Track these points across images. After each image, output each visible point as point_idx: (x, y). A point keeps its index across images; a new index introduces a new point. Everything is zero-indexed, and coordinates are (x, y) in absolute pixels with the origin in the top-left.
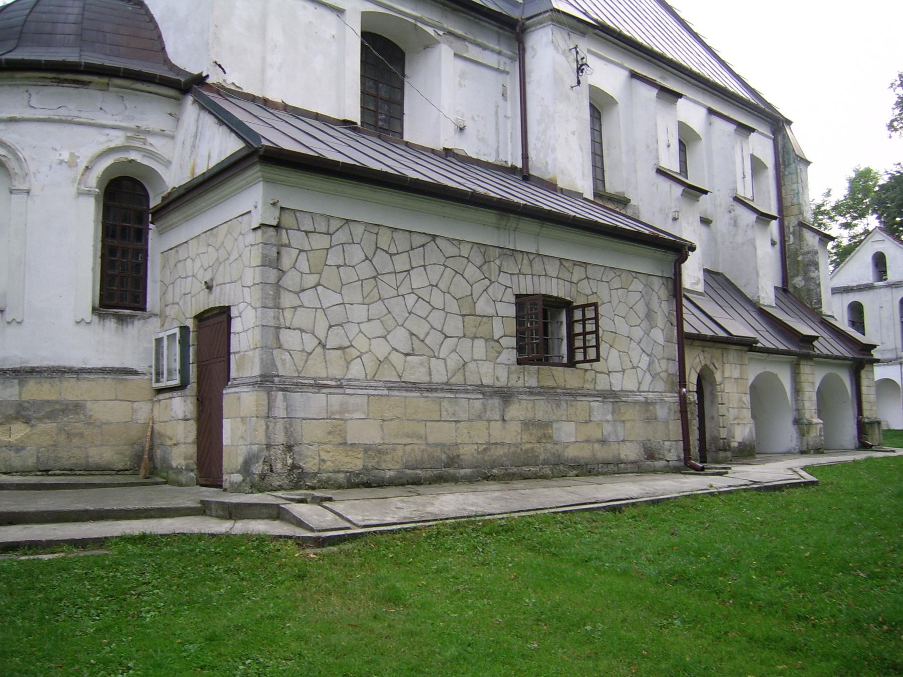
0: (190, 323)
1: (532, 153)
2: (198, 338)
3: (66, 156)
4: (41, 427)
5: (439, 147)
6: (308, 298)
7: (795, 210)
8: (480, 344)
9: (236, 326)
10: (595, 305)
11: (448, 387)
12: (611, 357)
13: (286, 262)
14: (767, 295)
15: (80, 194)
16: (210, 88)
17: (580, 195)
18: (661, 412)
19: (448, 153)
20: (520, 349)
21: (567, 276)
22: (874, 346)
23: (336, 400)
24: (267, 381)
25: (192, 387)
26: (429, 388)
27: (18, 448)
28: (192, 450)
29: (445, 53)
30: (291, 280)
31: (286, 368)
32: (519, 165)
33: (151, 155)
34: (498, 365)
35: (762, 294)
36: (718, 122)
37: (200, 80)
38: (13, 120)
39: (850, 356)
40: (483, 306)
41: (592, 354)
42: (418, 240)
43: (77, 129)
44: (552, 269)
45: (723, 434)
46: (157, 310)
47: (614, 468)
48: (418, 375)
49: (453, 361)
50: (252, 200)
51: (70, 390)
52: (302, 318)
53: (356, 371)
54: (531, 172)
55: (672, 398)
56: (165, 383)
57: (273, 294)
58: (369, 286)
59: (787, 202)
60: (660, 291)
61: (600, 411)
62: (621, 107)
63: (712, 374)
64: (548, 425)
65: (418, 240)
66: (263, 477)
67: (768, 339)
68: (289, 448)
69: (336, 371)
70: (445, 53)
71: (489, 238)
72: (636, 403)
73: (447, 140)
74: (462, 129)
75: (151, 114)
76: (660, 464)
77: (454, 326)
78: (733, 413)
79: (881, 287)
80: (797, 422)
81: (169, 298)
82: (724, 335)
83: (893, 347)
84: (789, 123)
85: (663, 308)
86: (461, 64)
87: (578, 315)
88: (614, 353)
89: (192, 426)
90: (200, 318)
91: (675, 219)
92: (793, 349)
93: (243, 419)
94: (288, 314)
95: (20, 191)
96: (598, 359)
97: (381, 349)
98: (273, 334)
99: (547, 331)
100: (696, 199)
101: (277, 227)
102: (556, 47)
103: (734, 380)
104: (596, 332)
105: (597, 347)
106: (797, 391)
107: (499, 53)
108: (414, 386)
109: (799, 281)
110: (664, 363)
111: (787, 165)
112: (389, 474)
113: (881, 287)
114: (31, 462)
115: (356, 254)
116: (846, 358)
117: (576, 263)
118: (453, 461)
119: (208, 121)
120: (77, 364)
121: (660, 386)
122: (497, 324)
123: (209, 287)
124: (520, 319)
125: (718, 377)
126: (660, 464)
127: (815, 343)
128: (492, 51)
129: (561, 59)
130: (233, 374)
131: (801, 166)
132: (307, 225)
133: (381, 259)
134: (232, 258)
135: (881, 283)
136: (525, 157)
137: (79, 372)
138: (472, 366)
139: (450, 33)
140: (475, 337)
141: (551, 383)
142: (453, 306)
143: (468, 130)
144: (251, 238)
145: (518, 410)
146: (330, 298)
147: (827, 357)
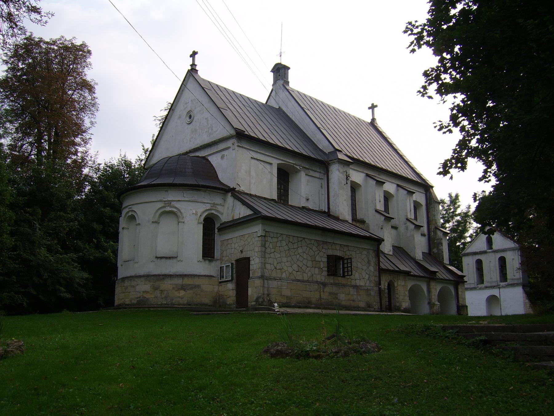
0: (234, 262)
1: (331, 207)
2: (236, 268)
3: (194, 212)
4: (188, 292)
5: (301, 206)
6: (272, 255)
7: (434, 223)
8: (317, 269)
9: (252, 262)
10: (351, 258)
11: (308, 281)
12: (356, 275)
13: (267, 246)
14: (419, 256)
15: (199, 223)
16: (236, 192)
17: (347, 221)
18: (372, 293)
19: (304, 208)
20: (328, 271)
21: (342, 249)
22: (465, 276)
23: (279, 283)
24: (262, 277)
25: (235, 280)
26: (302, 281)
27: (182, 298)
28: (234, 298)
29: (303, 174)
30: (268, 250)
31: (267, 274)
32: (327, 211)
33: (217, 211)
34: (322, 276)
35: (417, 256)
36: (401, 190)
37: (234, 189)
38: (179, 201)
39: (452, 279)
40: (318, 258)
41: (350, 273)
42: (300, 239)
43: (196, 203)
44: (338, 247)
45: (398, 304)
46: (219, 258)
47: (358, 308)
48: (300, 278)
49: (309, 274)
50: (258, 229)
51: (197, 281)
52: (270, 261)
53: (284, 275)
54: (331, 214)
55: (376, 289)
56: (224, 279)
57: (264, 254)
58: (287, 252)
59: (431, 219)
60: (372, 255)
61: (352, 291)
62: (363, 189)
63: (393, 283)
64: (336, 294)
65: (300, 239)
66: (262, 302)
67: (416, 271)
68: (268, 295)
69: (279, 275)
70: (303, 174)
71: (319, 238)
72: (364, 289)
73: (303, 203)
74: (308, 200)
75: (218, 199)
76: (372, 309)
77: (310, 264)
78: (401, 298)
79: (490, 252)
80: (429, 303)
81: (225, 254)
82: (398, 270)
83: (496, 280)
84: (432, 187)
85: (373, 260)
86: (308, 177)
87: (346, 261)
88: (357, 274)
89: (235, 291)
90: (237, 261)
91: (382, 228)
92: (426, 275)
93: (256, 287)
94: (267, 260)
95: (181, 222)
96: (352, 275)
97: (290, 270)
98: (263, 267)
99: (337, 266)
100: (390, 221)
101: (265, 236)
102: (339, 171)
103: (402, 288)
104: (351, 267)
105: (351, 271)
106: (429, 291)
107: (320, 173)
108: (299, 281)
109: (435, 250)
110: (373, 278)
111: (431, 204)
112: (293, 304)
113: (490, 252)
114: (186, 302)
115: (284, 243)
116: (451, 280)
117: (345, 246)
118: (310, 302)
119: (238, 204)
120: (198, 274)
121: (372, 285)
122: (321, 263)
123: (242, 252)
124: (328, 262)
125: (396, 284)
126: (372, 309)
127: (437, 274)
128: (318, 172)
129: (341, 175)
130: (251, 276)
131: (437, 205)
132: (272, 235)
133: (290, 244)
134: (250, 244)
135: (490, 250)
136: (329, 208)
137: (199, 276)
138: (315, 276)
139: (304, 168)
140: (315, 268)
141: (337, 282)
142: (309, 258)
143: (310, 200)
144: (257, 239)
145: (327, 289)
146: (278, 256)
147: (442, 279)
